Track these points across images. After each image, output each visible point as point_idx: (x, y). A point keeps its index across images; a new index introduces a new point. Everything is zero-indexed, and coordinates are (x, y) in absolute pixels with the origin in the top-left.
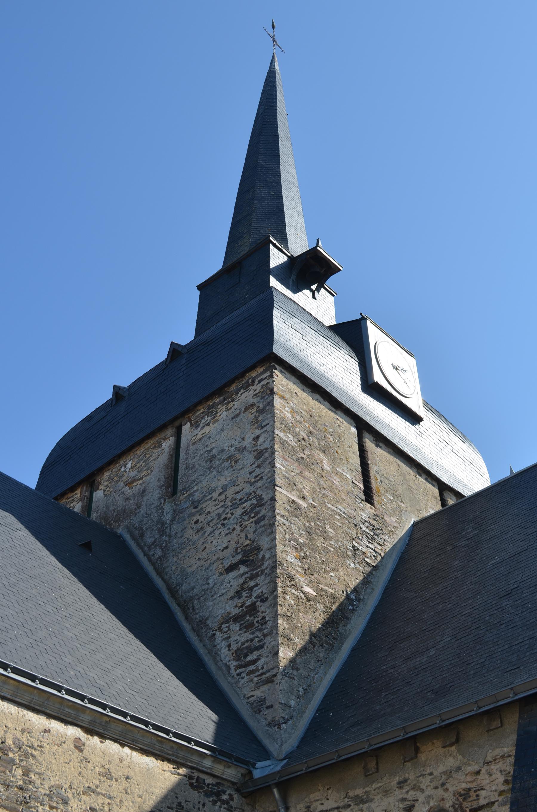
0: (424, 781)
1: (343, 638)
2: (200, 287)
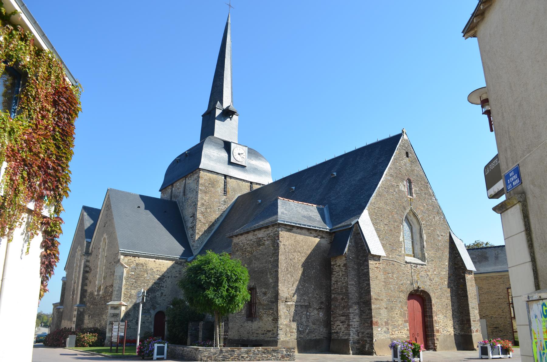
0: (91, 341)
1: (212, 230)
2: (160, 191)
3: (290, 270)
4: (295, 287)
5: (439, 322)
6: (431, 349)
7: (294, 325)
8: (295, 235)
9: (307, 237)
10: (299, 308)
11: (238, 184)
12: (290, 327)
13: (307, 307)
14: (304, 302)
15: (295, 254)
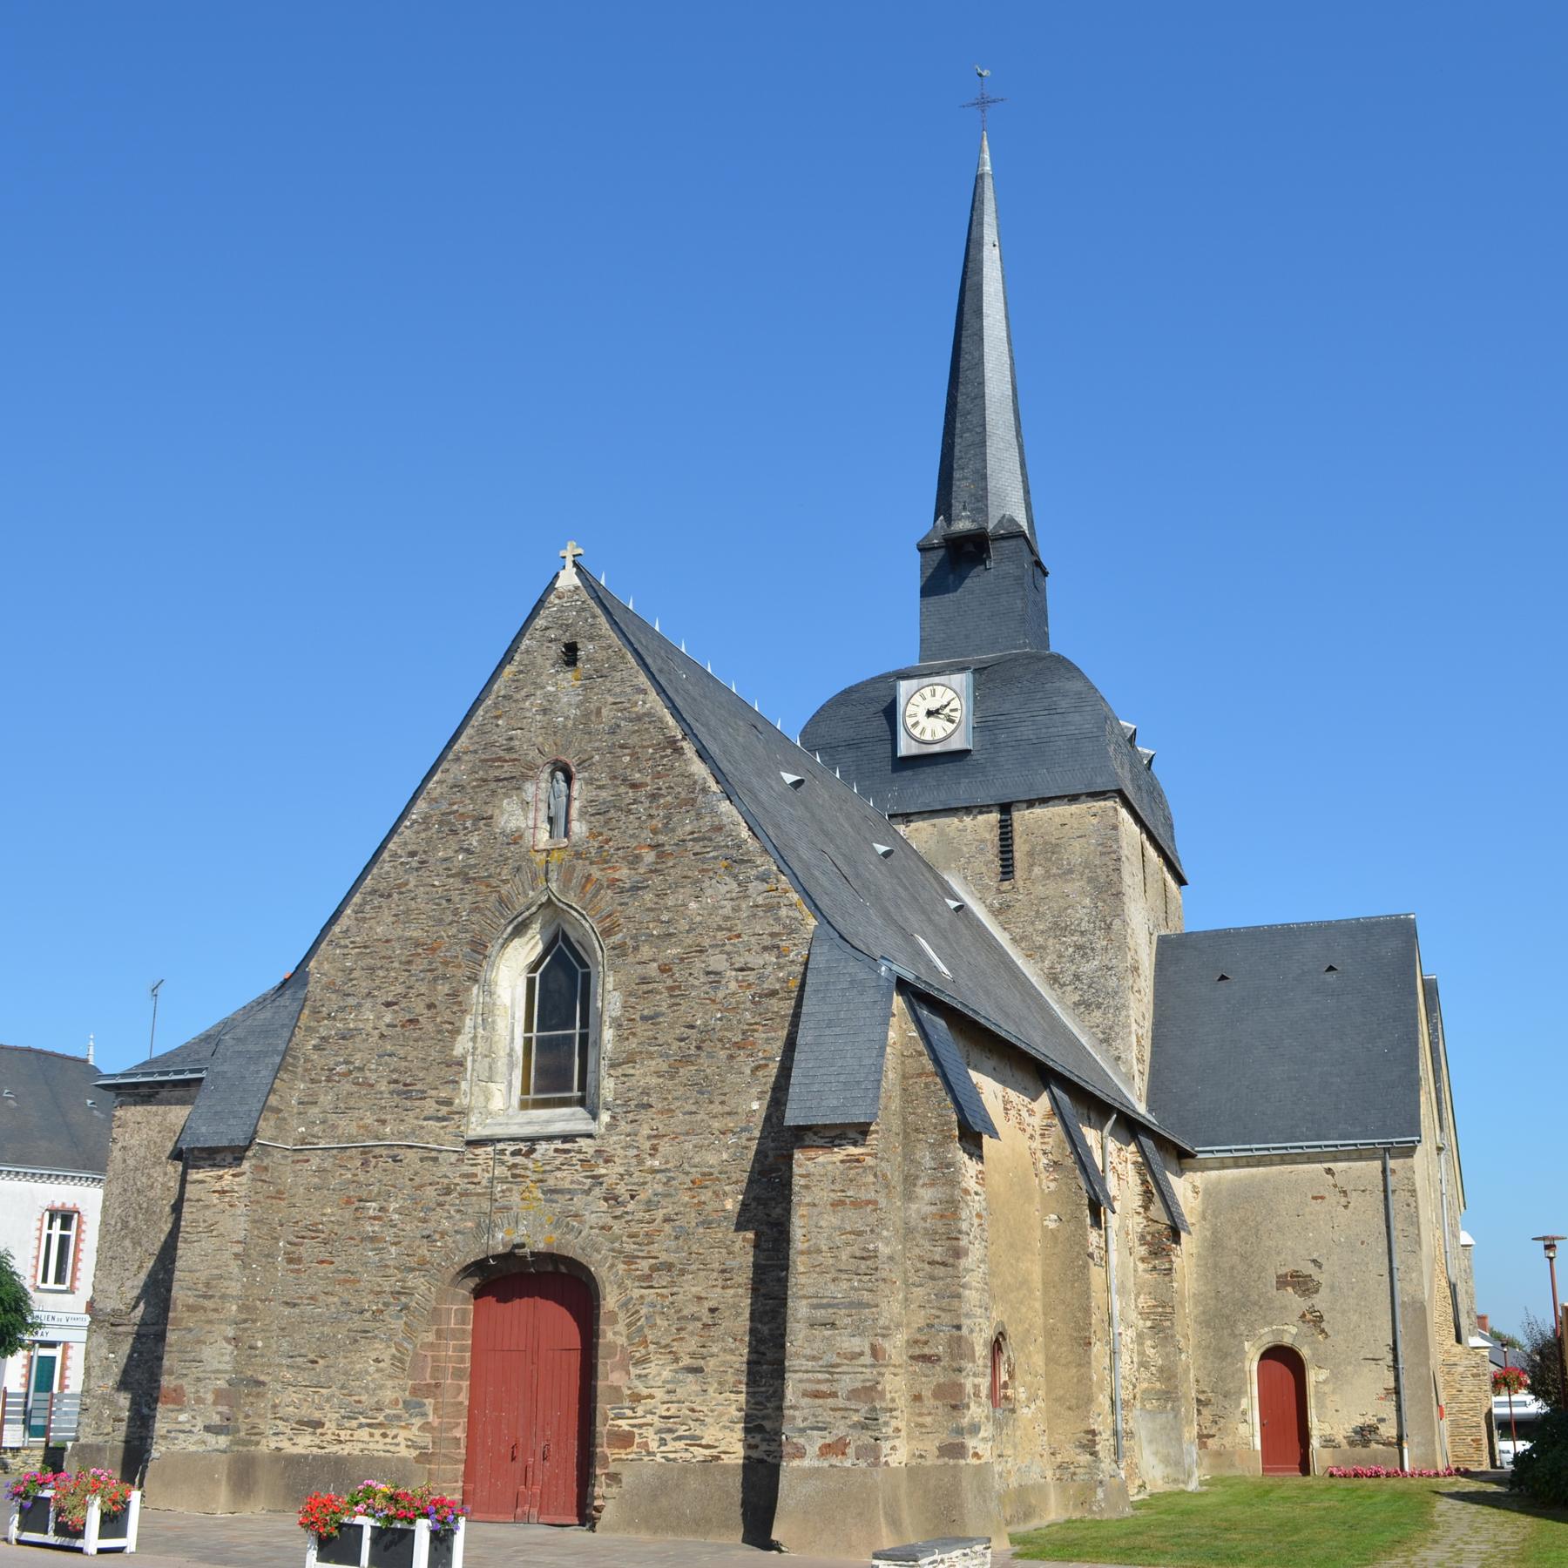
3: (132, 1224)
5: (637, 1398)
11: (942, 833)
12: (111, 1403)
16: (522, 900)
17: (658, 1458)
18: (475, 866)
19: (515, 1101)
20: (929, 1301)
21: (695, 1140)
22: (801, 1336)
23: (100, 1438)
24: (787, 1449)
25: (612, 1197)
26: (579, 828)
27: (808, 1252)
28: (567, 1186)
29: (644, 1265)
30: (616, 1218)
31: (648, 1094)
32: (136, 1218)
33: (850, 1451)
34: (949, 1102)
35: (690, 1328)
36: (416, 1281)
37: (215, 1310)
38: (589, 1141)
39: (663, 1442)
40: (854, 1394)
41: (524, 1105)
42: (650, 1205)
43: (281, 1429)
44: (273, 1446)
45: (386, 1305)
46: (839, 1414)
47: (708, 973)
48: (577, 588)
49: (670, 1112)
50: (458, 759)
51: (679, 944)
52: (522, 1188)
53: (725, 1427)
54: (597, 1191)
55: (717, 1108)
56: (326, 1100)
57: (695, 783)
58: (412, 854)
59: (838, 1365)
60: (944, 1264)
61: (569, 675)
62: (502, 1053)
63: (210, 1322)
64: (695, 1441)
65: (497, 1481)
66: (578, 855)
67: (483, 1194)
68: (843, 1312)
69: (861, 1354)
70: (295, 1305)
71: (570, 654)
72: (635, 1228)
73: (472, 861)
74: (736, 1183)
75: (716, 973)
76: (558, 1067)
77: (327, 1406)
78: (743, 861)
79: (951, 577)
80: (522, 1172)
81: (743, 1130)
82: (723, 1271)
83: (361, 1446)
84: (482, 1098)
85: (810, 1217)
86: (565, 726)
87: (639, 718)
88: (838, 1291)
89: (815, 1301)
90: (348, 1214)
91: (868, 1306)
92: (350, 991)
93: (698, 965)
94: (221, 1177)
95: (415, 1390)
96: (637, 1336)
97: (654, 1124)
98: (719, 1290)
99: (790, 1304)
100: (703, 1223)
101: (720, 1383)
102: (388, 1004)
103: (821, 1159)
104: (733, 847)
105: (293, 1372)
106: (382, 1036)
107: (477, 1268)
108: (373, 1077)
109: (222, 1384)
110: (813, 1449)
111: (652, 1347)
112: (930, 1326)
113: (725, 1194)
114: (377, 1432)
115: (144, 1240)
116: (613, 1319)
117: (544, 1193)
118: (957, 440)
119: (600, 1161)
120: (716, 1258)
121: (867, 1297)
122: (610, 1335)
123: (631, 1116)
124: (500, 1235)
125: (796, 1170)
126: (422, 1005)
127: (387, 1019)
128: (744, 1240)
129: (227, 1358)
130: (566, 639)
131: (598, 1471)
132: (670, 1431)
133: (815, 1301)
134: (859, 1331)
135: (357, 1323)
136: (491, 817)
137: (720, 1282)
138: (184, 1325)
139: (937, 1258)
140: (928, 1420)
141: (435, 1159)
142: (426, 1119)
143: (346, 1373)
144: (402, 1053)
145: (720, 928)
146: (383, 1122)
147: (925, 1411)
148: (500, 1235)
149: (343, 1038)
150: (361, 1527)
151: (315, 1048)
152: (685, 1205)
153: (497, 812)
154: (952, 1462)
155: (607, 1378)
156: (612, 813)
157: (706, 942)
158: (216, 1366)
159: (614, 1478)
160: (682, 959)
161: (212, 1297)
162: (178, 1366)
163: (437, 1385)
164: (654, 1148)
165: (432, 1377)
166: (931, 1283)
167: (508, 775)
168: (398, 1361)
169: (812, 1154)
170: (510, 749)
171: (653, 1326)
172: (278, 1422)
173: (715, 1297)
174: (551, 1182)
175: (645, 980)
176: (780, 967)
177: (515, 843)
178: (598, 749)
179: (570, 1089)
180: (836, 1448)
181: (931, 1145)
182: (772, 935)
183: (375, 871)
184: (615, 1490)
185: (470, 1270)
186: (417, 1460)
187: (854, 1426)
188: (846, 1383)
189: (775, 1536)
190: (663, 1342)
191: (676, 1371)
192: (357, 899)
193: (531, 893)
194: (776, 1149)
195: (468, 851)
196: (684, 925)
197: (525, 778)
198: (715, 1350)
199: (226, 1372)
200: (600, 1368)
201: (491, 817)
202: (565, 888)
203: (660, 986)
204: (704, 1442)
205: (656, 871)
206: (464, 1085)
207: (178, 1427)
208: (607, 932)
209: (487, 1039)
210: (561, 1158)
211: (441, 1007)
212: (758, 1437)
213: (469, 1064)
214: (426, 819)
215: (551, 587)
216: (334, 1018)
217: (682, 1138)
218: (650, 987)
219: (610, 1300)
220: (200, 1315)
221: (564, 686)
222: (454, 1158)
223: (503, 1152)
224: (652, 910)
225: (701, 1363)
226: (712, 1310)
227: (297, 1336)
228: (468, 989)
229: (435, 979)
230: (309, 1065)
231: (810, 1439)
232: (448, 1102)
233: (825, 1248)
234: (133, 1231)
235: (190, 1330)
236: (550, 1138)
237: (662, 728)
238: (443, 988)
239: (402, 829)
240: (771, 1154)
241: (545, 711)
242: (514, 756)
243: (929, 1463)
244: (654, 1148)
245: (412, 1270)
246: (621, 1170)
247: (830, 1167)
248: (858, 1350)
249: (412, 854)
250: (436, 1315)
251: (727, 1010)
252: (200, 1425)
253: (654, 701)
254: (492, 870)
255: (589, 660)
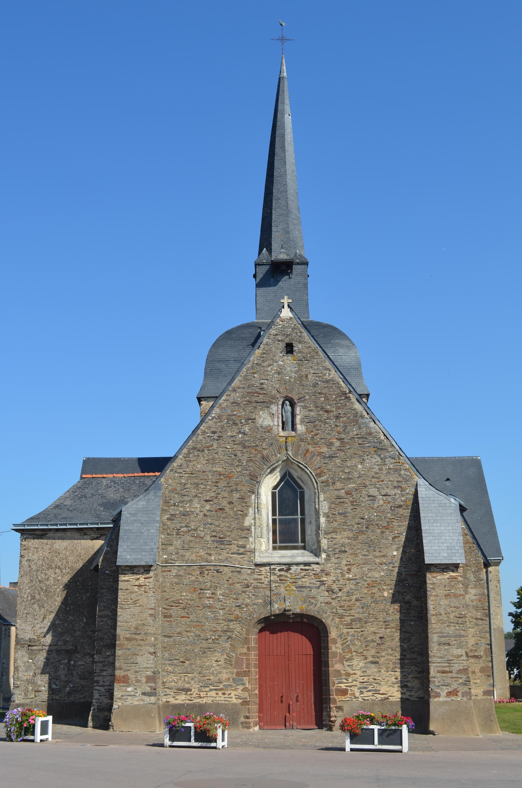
3: (37, 597)
4: (47, 623)
5: (348, 675)
6: (326, 726)
7: (43, 682)
8: (50, 542)
9: (76, 541)
10: (54, 654)
13: (70, 653)
14: (65, 644)
15: (50, 572)
16: (274, 458)
17: (360, 699)
18: (248, 441)
19: (271, 547)
20: (476, 634)
21: (368, 567)
22: (435, 649)
23: (28, 700)
24: (432, 694)
25: (330, 590)
26: (300, 427)
27: (436, 615)
28: (308, 585)
29: (348, 619)
30: (333, 599)
31: (344, 547)
32: (39, 594)
33: (460, 694)
34: (480, 553)
35: (371, 645)
36: (236, 626)
37: (143, 640)
38: (317, 566)
39: (362, 693)
40: (459, 671)
41: (274, 548)
42: (348, 594)
43: (169, 693)
44: (164, 700)
45: (220, 636)
46: (453, 680)
47: (369, 496)
48: (291, 318)
49: (356, 555)
50: (234, 390)
51: (355, 482)
52: (286, 585)
53: (390, 686)
54: (322, 587)
55: (377, 554)
56: (177, 543)
57: (357, 413)
58: (214, 433)
59: (452, 660)
60: (482, 619)
61: (290, 358)
62: (265, 525)
63: (140, 645)
64: (377, 692)
65: (274, 712)
66: (302, 440)
67: (267, 588)
68: (453, 639)
69: (462, 656)
70: (170, 637)
71: (289, 349)
72: (342, 604)
73: (247, 439)
74: (388, 585)
75: (373, 496)
76: (287, 534)
77: (192, 682)
78: (382, 449)
79: (272, 279)
80: (285, 579)
81: (390, 563)
82: (385, 622)
83: (212, 699)
84: (259, 545)
85: (436, 600)
86: (290, 381)
87: (327, 381)
88: (451, 630)
89: (440, 635)
90: (195, 596)
91: (463, 636)
92: (185, 493)
93: (364, 492)
94: (138, 579)
95: (238, 674)
96: (347, 648)
97: (348, 559)
98: (383, 629)
99: (430, 636)
100: (374, 601)
101: (386, 668)
102: (207, 501)
103: (439, 577)
104: (377, 443)
105: (172, 667)
106: (205, 515)
107: (266, 620)
108: (202, 534)
109: (149, 673)
110: (443, 694)
111: (354, 653)
112: (477, 644)
113: (384, 590)
114: (220, 693)
115: (45, 605)
116: (335, 642)
117: (296, 587)
118: (273, 212)
119: (323, 575)
120: (381, 616)
121: (463, 633)
122: (334, 649)
123: (337, 556)
124: (276, 606)
125: (428, 581)
126: (226, 502)
127: (208, 507)
128: (394, 608)
129: (151, 662)
130: (287, 340)
131: (332, 706)
132: (365, 688)
133: (440, 635)
134: (460, 646)
135: (205, 644)
136: (255, 419)
137: (384, 626)
138: (125, 647)
139: (479, 617)
140: (478, 681)
141: (239, 572)
142: (232, 554)
143: (201, 667)
144: (217, 523)
145: (373, 477)
146: (210, 555)
147: (477, 677)
148: (276, 606)
149: (184, 515)
150: (373, 730)
151: (168, 519)
152: (366, 594)
153: (257, 417)
154: (489, 697)
155: (333, 667)
156: (317, 423)
157: (368, 483)
158: (145, 665)
159: (340, 708)
160: (356, 490)
161: (139, 634)
162: (123, 666)
163: (249, 671)
164: (349, 570)
165: (246, 668)
166: (477, 627)
167: (262, 400)
168: (228, 661)
169: (435, 575)
170: (262, 389)
171: (354, 645)
172: (166, 690)
173: (382, 632)
174: (300, 583)
175: (339, 497)
176: (403, 496)
177: (269, 432)
178: (307, 393)
179: (297, 542)
180: (453, 693)
181: (473, 571)
182: (398, 482)
183: (194, 439)
184: (340, 713)
185: (260, 621)
186: (242, 704)
187: (460, 684)
188: (456, 667)
189: (432, 728)
190: (359, 651)
191: (366, 663)
192: (185, 451)
193: (279, 455)
194: (406, 571)
195: (244, 434)
196: (356, 475)
197: (271, 403)
198: (383, 654)
199: (151, 668)
200: (330, 662)
201: (255, 419)
202: (296, 454)
203: (347, 500)
204: (381, 692)
205: (341, 450)
206: (251, 539)
207: (127, 693)
208: (319, 475)
209: (259, 519)
210: (304, 573)
211: (236, 504)
212: (405, 690)
213: (253, 530)
214: (220, 417)
215: (277, 316)
216: (178, 506)
217: (362, 566)
218: (342, 500)
219: (333, 634)
220: (133, 642)
221: (289, 363)
222: (249, 571)
223: (274, 569)
224: (340, 467)
225: (378, 659)
226: (381, 638)
227: (173, 651)
228: (250, 496)
229: (232, 491)
230: (166, 527)
231: (442, 690)
232: (244, 547)
233: (443, 613)
234: (39, 601)
235: (129, 649)
236: (298, 564)
237: (339, 387)
238: (236, 495)
239: (207, 420)
240: (403, 573)
241: (279, 373)
242: (265, 392)
243: (479, 698)
244: (349, 570)
245: (231, 621)
246: (334, 579)
247: (443, 581)
248: (460, 654)
249: (214, 433)
250: (246, 641)
251: (379, 512)
252: (139, 691)
253: (334, 374)
254: (257, 443)
255: (299, 352)
